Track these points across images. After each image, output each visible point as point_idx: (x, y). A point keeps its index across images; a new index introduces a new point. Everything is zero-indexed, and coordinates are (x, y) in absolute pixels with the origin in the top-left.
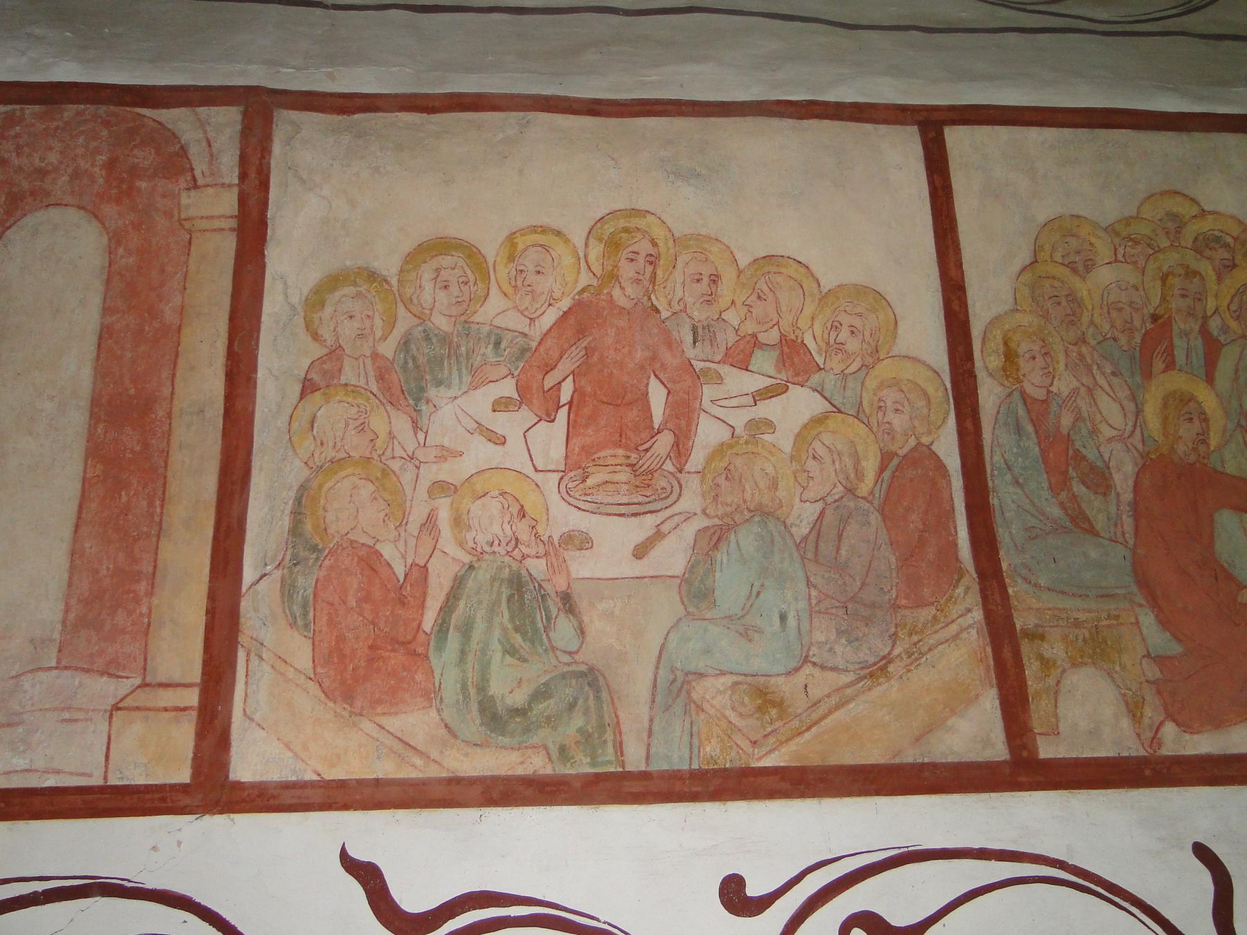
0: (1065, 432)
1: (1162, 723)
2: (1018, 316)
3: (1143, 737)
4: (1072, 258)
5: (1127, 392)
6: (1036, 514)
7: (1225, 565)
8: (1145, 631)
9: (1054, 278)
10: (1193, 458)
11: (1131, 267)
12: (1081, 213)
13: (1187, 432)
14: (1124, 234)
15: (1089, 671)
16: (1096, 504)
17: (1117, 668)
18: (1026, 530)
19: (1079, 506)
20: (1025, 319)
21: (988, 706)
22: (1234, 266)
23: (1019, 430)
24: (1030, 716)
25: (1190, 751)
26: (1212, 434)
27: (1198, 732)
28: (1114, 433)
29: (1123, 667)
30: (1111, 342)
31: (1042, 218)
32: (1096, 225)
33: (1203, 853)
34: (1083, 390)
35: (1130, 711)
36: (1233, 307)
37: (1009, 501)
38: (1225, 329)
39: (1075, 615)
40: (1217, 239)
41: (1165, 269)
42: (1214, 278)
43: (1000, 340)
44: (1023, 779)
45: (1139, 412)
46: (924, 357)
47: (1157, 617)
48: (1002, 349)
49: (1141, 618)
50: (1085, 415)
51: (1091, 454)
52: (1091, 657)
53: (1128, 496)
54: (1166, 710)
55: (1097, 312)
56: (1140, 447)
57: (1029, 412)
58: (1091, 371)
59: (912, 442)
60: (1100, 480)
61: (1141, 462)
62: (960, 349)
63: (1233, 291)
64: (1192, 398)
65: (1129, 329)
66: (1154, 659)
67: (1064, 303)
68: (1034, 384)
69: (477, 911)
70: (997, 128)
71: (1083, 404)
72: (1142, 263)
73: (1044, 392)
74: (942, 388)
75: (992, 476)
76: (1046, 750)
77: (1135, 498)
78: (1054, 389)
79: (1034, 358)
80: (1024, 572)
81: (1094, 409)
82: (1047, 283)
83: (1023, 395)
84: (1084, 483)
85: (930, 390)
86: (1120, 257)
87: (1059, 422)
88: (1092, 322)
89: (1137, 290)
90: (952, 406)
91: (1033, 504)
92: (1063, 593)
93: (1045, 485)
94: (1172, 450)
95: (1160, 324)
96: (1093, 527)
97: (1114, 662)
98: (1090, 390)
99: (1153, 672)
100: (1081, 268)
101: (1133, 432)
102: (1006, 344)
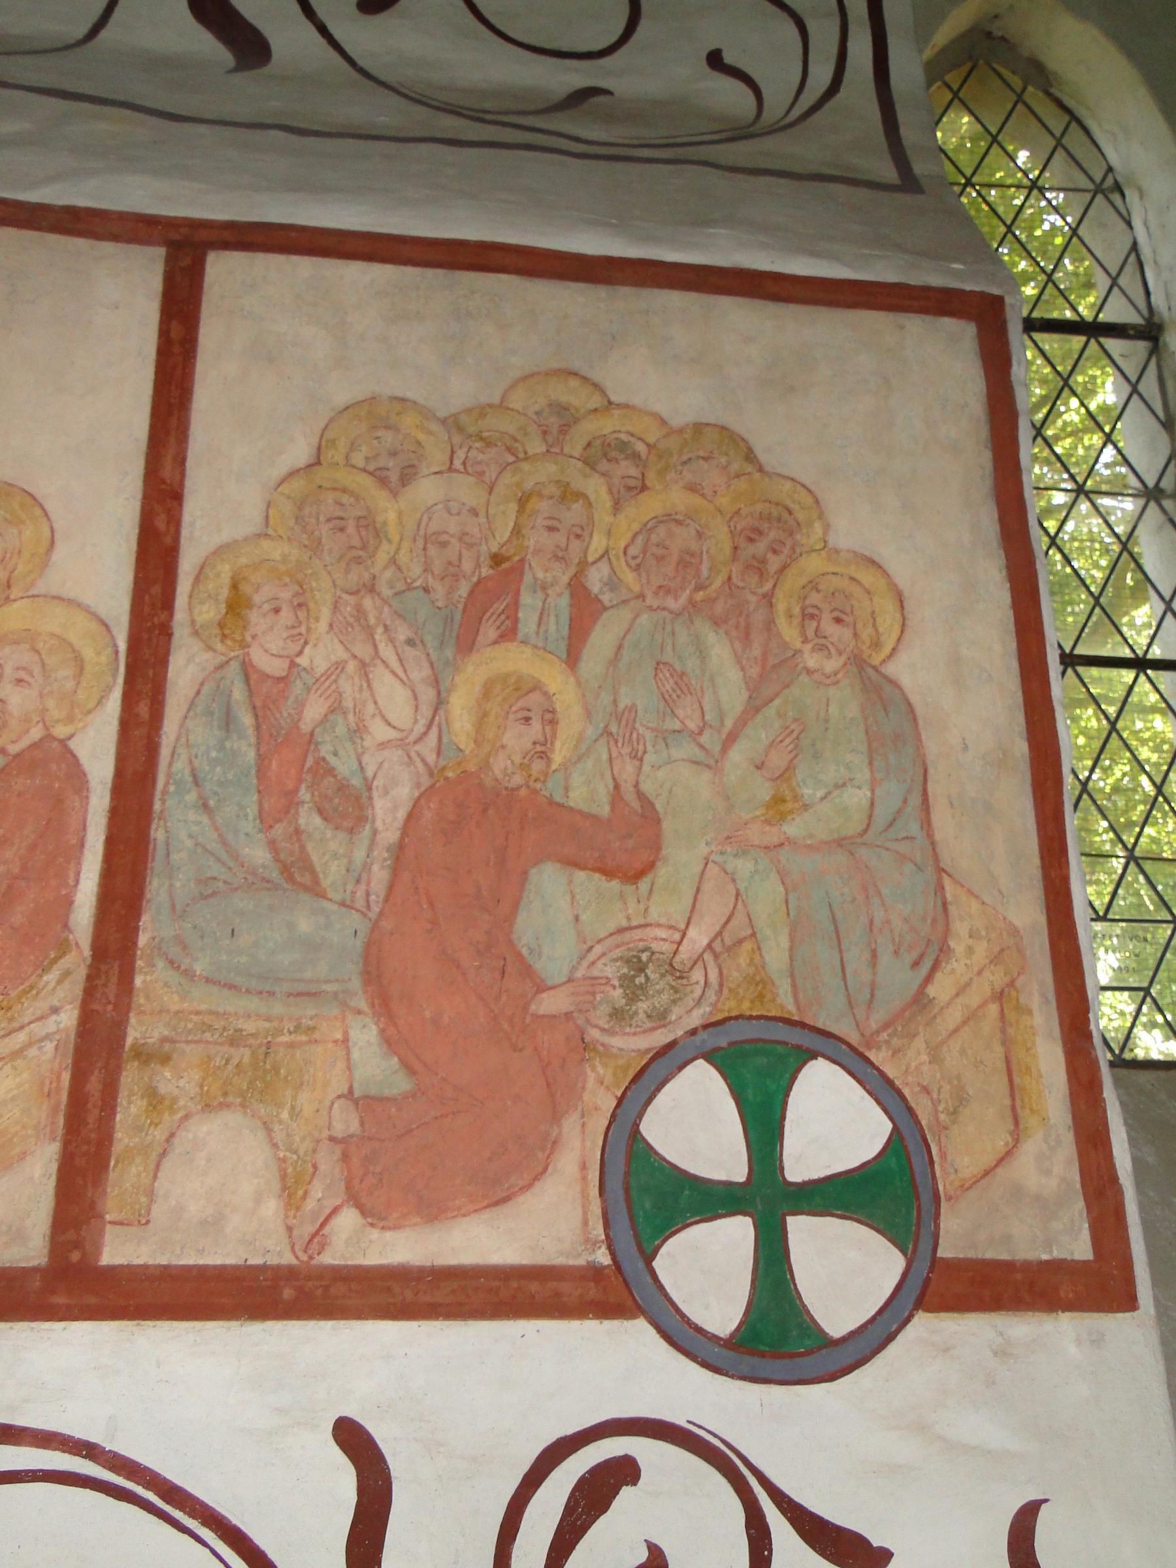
0: (305, 727)
1: (335, 1211)
2: (266, 544)
3: (295, 1232)
4: (382, 463)
5: (426, 672)
6: (224, 856)
7: (525, 951)
8: (356, 1055)
9: (344, 490)
10: (517, 780)
11: (472, 479)
12: (409, 395)
13: (517, 739)
14: (472, 430)
15: (233, 1118)
16: (333, 845)
17: (285, 1115)
18: (199, 881)
19: (303, 848)
20: (275, 550)
21: (37, 1173)
22: (644, 488)
23: (228, 722)
24: (104, 1192)
25: (372, 1259)
26: (558, 744)
27: (396, 1227)
28: (392, 734)
29: (295, 1114)
30: (421, 593)
31: (342, 397)
32: (426, 413)
33: (352, 1438)
34: (352, 666)
35: (284, 1188)
36: (632, 551)
37: (183, 835)
38: (613, 583)
39: (241, 1024)
40: (623, 446)
41: (529, 485)
42: (609, 504)
43: (226, 580)
44: (59, 1300)
45: (440, 703)
46: (88, 599)
47: (382, 1031)
48: (225, 593)
49: (354, 1034)
50: (348, 703)
51: (344, 766)
52: (242, 1094)
53: (390, 835)
54: (348, 1187)
55: (406, 545)
56: (431, 758)
57: (251, 693)
58: (372, 636)
59: (36, 733)
60: (349, 807)
61: (426, 782)
62: (156, 590)
63: (636, 527)
64: (537, 687)
65: (452, 575)
66: (356, 1102)
67: (351, 529)
68: (268, 651)
69: (58, 1454)
70: (295, 258)
71: (348, 687)
72: (491, 473)
73: (285, 664)
74: (109, 650)
75: (165, 792)
76: (118, 1250)
77: (402, 838)
78: (303, 661)
79: (277, 611)
80: (174, 951)
81: (366, 694)
82: (330, 497)
83: (247, 668)
84: (320, 812)
85: (88, 653)
86: (457, 464)
87: (300, 713)
88: (393, 561)
89: (476, 515)
90: (121, 680)
91: (224, 843)
92: (231, 987)
93: (252, 811)
94: (486, 765)
95: (506, 570)
96: (316, 882)
97: (280, 1106)
98: (363, 665)
99: (346, 1122)
100: (394, 477)
101: (425, 734)
102: (235, 586)
